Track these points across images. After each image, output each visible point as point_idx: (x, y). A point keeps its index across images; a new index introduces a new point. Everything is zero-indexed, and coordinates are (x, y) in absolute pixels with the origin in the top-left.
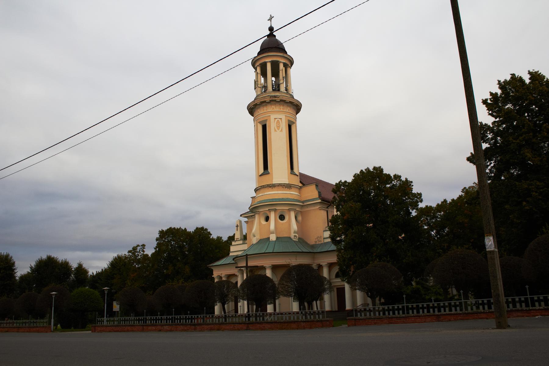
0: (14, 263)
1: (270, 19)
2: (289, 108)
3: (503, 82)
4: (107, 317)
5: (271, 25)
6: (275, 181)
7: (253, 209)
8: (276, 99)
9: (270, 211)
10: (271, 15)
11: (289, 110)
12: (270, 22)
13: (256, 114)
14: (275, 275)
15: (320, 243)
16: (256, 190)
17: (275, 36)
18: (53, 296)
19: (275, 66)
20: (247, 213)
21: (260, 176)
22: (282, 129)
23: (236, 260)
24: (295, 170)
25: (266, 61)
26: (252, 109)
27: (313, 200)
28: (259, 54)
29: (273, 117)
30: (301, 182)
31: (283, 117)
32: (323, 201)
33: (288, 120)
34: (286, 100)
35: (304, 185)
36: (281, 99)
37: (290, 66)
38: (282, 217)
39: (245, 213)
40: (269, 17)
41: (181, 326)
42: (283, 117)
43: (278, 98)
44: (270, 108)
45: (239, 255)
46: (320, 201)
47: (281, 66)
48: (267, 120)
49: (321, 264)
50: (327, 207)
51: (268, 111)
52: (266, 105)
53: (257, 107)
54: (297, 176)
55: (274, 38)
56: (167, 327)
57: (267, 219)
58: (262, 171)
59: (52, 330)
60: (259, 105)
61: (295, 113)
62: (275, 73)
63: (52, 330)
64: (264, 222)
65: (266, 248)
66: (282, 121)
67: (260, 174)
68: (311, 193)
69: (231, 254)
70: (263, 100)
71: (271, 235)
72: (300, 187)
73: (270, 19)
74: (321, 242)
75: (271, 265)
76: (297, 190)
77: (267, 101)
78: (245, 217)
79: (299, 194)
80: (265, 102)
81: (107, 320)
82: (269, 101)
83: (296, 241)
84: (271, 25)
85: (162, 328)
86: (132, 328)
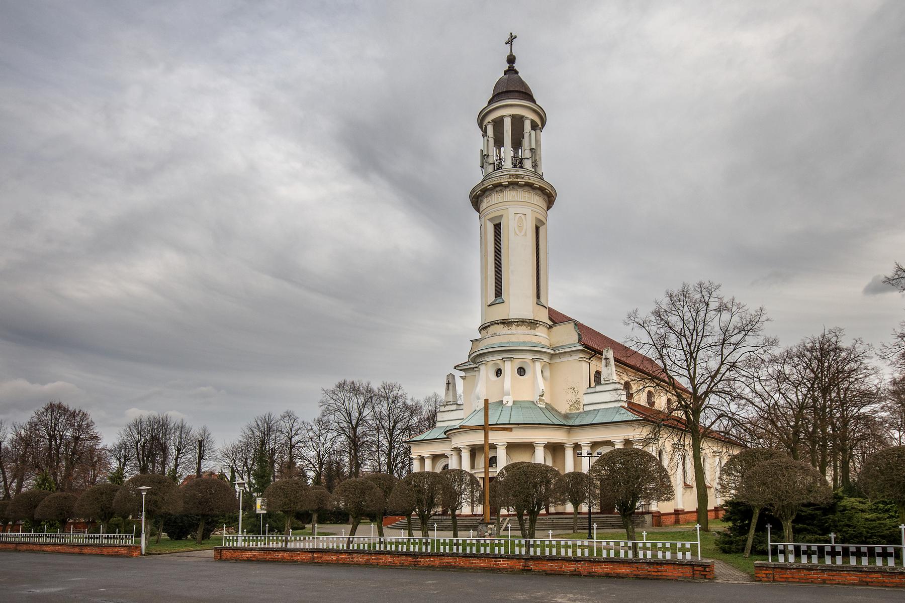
1: (511, 40)
2: (537, 198)
4: (243, 532)
6: (514, 315)
7: (476, 357)
8: (518, 180)
9: (504, 361)
10: (511, 34)
11: (537, 201)
12: (509, 48)
13: (483, 206)
15: (577, 412)
16: (483, 328)
17: (517, 73)
18: (143, 493)
19: (518, 122)
20: (464, 364)
21: (489, 306)
23: (450, 434)
24: (542, 300)
26: (477, 199)
27: (570, 346)
28: (490, 102)
29: (512, 210)
30: (550, 318)
31: (528, 211)
32: (586, 348)
33: (536, 218)
34: (534, 182)
35: (555, 323)
36: (527, 181)
37: (540, 126)
38: (521, 371)
39: (462, 364)
40: (507, 39)
41: (388, 557)
42: (528, 211)
43: (523, 178)
44: (509, 195)
45: (455, 426)
46: (581, 347)
47: (527, 125)
48: (502, 215)
50: (590, 358)
52: (502, 191)
53: (487, 193)
54: (546, 308)
55: (516, 75)
56: (359, 556)
57: (499, 372)
58: (491, 298)
59: (144, 553)
60: (491, 189)
63: (144, 553)
64: (493, 377)
65: (498, 417)
67: (488, 304)
68: (567, 336)
69: (438, 425)
70: (498, 182)
71: (505, 397)
72: (549, 325)
73: (511, 40)
74: (579, 411)
76: (546, 329)
77: (503, 184)
78: (461, 370)
79: (548, 338)
80: (500, 185)
81: (243, 538)
82: (507, 183)
83: (543, 408)
85: (349, 558)
86: (292, 556)
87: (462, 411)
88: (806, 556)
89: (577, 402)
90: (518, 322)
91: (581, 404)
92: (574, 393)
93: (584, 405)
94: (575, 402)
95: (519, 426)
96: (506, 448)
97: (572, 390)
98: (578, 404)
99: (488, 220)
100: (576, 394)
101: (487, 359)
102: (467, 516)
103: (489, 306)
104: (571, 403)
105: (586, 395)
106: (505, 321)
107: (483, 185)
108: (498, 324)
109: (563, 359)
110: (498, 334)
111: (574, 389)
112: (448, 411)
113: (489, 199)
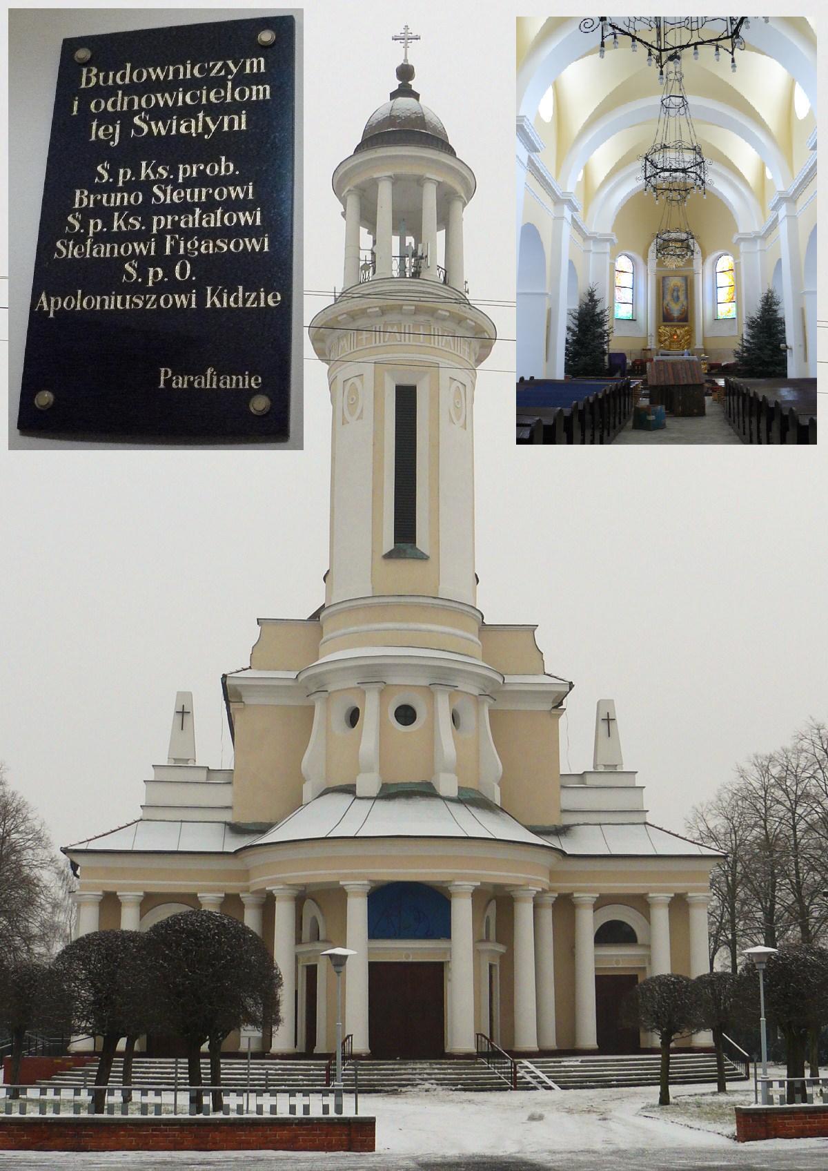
0: (555, 825)
3: (612, 356)
5: (406, 60)
14: (319, 906)
19: (408, 188)
22: (362, 411)
25: (375, 176)
28: (359, 149)
49: (341, 883)
51: (374, 345)
57: (354, 717)
58: (388, 543)
61: (473, 358)
62: (408, 222)
66: (362, 382)
75: (366, 882)
77: (369, 310)
84: (406, 60)
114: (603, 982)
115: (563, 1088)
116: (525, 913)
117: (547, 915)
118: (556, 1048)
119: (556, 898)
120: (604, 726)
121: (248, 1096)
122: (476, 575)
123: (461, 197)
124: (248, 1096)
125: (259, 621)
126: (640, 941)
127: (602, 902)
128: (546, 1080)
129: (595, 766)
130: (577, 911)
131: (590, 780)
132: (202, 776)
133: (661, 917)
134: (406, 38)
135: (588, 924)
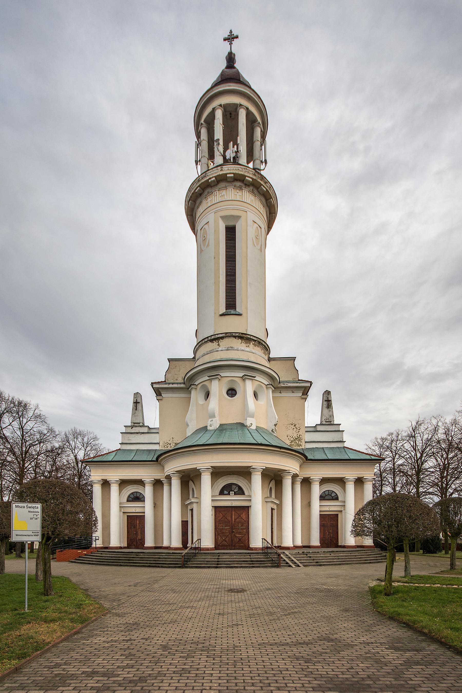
21: (221, 315)
52: (241, 188)
53: (222, 185)
57: (232, 392)
58: (223, 309)
67: (220, 314)
70: (242, 173)
87: (157, 435)
88: (14, 538)
89: (299, 438)
90: (255, 341)
91: (303, 441)
92: (295, 429)
93: (306, 442)
94: (296, 439)
95: (282, 450)
96: (119, 485)
97: (293, 427)
98: (299, 440)
99: (221, 217)
100: (298, 430)
101: (223, 374)
102: (208, 549)
103: (221, 315)
104: (292, 439)
105: (308, 433)
106: (244, 336)
107: (222, 170)
108: (235, 337)
109: (283, 394)
110: (235, 348)
111: (295, 426)
112: (137, 433)
113: (224, 192)
114: (322, 517)
115: (305, 566)
116: (287, 482)
117: (298, 487)
118: (301, 545)
119: (303, 479)
120: (325, 403)
121: (407, 562)
122: (266, 329)
123: (259, 123)
124: (407, 562)
125: (170, 360)
126: (340, 499)
127: (324, 481)
128: (294, 559)
129: (321, 422)
130: (312, 486)
131: (319, 428)
132: (146, 430)
133: (350, 487)
134: (231, 38)
135: (316, 490)
